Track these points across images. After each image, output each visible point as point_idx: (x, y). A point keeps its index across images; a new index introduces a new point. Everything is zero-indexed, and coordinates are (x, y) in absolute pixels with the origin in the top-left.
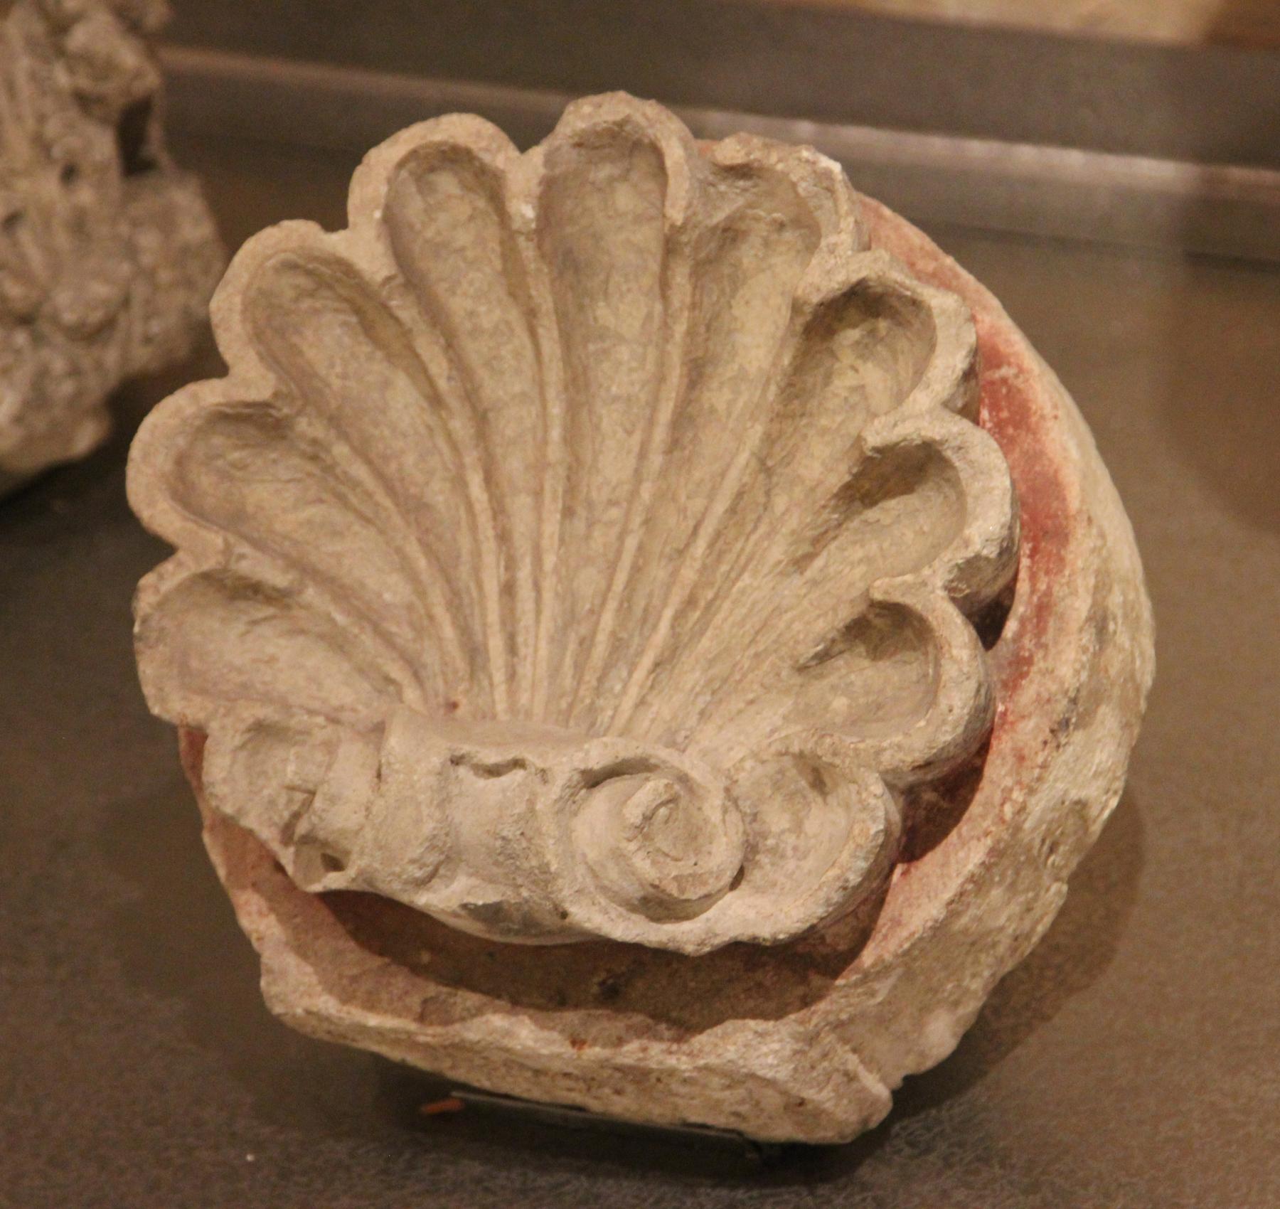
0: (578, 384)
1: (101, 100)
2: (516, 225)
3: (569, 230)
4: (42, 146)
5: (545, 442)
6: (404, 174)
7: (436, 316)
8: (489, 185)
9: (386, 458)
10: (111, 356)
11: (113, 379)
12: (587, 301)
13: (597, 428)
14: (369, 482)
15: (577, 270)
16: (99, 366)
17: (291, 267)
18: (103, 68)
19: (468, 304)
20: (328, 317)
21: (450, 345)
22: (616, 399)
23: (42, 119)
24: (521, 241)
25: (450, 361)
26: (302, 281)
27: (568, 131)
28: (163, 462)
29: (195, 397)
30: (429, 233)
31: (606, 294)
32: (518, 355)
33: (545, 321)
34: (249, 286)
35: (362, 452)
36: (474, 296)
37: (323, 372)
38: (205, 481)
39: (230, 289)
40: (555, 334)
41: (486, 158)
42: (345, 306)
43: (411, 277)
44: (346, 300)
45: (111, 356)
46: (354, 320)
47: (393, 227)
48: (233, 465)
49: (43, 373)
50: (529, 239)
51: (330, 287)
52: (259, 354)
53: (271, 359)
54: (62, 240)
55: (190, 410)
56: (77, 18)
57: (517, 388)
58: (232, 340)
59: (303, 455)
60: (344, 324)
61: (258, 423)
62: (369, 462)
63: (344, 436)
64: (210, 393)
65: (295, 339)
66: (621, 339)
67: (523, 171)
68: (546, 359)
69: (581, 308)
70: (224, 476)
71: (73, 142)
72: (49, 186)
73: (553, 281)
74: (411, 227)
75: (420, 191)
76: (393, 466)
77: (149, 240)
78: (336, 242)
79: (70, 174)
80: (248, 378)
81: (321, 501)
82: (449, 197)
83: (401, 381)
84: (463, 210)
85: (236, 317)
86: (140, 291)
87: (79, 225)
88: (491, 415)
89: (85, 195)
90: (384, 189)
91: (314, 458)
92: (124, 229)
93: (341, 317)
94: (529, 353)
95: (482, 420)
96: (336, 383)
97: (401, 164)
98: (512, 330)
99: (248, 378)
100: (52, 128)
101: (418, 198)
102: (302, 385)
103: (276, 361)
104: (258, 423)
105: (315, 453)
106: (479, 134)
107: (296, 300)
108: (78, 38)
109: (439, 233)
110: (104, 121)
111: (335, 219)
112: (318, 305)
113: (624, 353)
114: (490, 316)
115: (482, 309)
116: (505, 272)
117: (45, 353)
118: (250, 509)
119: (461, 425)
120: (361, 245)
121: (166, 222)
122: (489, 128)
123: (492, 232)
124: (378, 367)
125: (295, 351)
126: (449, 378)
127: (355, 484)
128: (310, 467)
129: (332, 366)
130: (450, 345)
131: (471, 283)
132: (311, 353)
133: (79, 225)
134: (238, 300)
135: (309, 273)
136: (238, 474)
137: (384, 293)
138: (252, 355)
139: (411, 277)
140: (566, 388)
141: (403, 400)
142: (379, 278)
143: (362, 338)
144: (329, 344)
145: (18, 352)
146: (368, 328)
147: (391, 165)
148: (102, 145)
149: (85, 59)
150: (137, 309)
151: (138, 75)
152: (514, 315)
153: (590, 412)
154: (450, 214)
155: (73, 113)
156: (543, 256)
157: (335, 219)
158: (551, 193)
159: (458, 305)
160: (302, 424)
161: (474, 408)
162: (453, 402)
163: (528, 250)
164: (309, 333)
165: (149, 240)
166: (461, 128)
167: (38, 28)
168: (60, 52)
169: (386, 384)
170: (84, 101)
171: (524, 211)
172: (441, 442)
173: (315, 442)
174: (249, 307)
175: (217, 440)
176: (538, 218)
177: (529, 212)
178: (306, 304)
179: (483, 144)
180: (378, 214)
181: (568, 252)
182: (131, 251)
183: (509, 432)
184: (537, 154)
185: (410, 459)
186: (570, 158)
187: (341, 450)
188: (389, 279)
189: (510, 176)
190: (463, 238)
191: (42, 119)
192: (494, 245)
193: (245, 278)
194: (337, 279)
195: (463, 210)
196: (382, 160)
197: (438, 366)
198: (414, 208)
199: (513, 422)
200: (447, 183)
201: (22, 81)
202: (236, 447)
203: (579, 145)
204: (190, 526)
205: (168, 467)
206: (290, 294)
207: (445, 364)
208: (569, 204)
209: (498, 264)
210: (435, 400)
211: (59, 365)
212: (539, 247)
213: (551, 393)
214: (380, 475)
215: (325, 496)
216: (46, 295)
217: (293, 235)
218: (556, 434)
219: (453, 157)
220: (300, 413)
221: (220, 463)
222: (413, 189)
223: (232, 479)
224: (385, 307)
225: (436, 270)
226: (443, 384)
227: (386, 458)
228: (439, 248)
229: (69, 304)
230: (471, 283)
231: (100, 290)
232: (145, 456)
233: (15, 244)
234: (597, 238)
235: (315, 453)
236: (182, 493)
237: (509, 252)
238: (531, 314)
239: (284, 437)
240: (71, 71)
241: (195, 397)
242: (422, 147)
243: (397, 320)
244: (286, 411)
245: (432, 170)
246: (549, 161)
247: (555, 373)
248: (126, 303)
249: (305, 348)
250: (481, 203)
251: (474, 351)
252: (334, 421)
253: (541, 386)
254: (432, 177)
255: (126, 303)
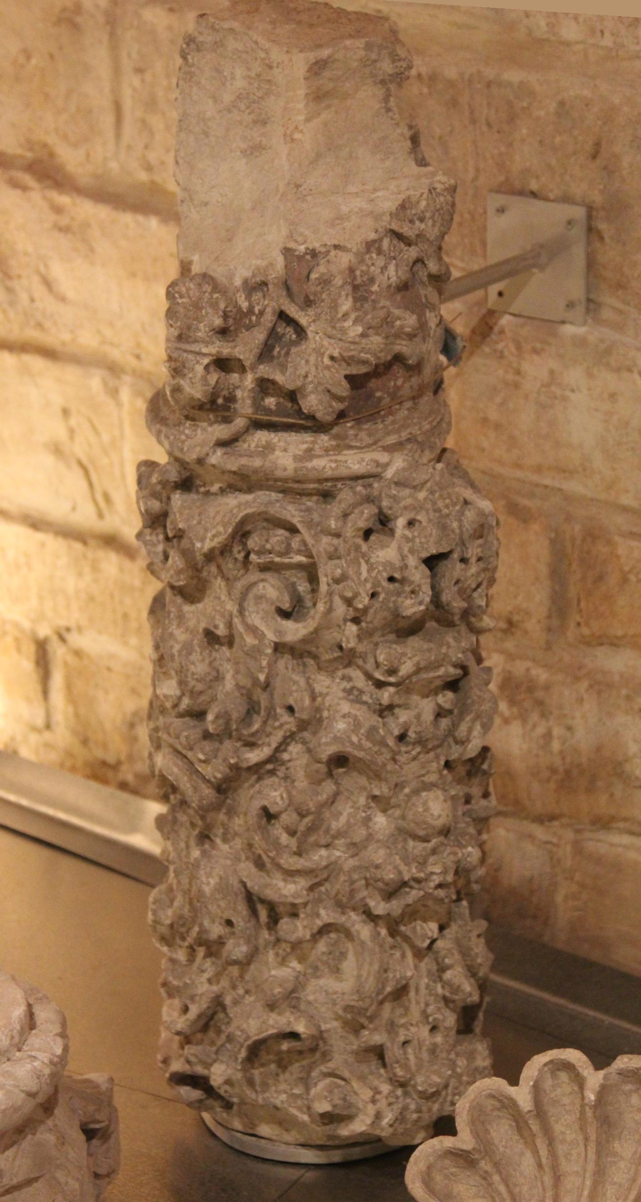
0: (600, 1174)
1: (454, 1001)
2: (586, 1101)
3: (609, 1108)
4: (425, 1015)
5: (581, 1195)
6: (546, 1069)
7: (547, 1130)
8: (580, 1082)
9: (515, 1185)
10: (436, 1107)
11: (434, 1118)
12: (611, 1139)
13: (604, 1194)
14: (505, 1194)
15: (609, 1126)
16: (430, 1110)
17: (492, 1096)
18: (457, 990)
19: (563, 1129)
20: (503, 1121)
21: (551, 1143)
22: (615, 1183)
23: (427, 1005)
24: (587, 1109)
25: (549, 1151)
26: (497, 1104)
27: (616, 1067)
28: (422, 1166)
29: (441, 1141)
30: (552, 1095)
31: (620, 1138)
32: (579, 1155)
33: (592, 1145)
34: (474, 1100)
35: (505, 1181)
36: (565, 1125)
37: (496, 1142)
38: (438, 1178)
39: (466, 1100)
40: (594, 1150)
41: (580, 1070)
42: (510, 1117)
43: (539, 1111)
44: (513, 1116)
45: (436, 1107)
46: (514, 1124)
47: (537, 1090)
48: (452, 1174)
49: (405, 1108)
50: (590, 1108)
51: (506, 1108)
52: (471, 1130)
53: (476, 1134)
54: (425, 1055)
55: (438, 1147)
56: (448, 967)
57: (575, 1169)
58: (461, 1123)
59: (481, 1176)
60: (510, 1125)
61: (465, 1159)
62: (507, 1186)
63: (500, 1173)
64: (447, 1142)
65: (489, 1127)
66: (622, 1158)
67: (594, 1079)
68: (588, 1160)
69: (608, 1141)
70: (446, 1177)
71: (438, 1016)
72: (425, 1031)
73: (597, 1128)
74: (545, 1091)
75: (552, 1077)
76: (517, 1190)
77: (461, 1062)
78: (512, 1091)
79: (434, 1029)
80: (464, 1139)
81: (485, 1197)
82: (563, 1082)
83: (528, 1154)
84: (568, 1089)
85: (465, 1112)
86: (453, 1082)
87: (433, 1050)
88: (562, 1178)
89: (439, 1039)
90: (536, 1073)
91: (485, 1179)
92: (453, 1056)
93: (510, 1122)
94: (583, 1155)
95: (557, 1179)
96: (501, 1149)
97: (545, 1065)
98: (578, 1144)
99: (464, 1139)
100: (430, 1010)
101: (550, 1080)
102: (486, 1147)
103: (478, 1136)
104: (465, 1159)
105: (485, 1176)
106: (579, 1059)
107: (492, 1110)
108: (448, 975)
109: (556, 1096)
110: (453, 1010)
111: (514, 1081)
112: (501, 1114)
113: (622, 1164)
114: (570, 1136)
115: (568, 1132)
116: (580, 1119)
117: (408, 1100)
118: (454, 1194)
119: (548, 1179)
120: (521, 1096)
121: (471, 1056)
122: (584, 1058)
123: (578, 1101)
124: (521, 1146)
125: (487, 1131)
126: (547, 1158)
127: (500, 1194)
128: (483, 1182)
129: (501, 1141)
130: (551, 1143)
131: (565, 1120)
132: (493, 1134)
133: (433, 1050)
134: (468, 1105)
135: (500, 1101)
136: (453, 1178)
137: (527, 1116)
138: (468, 1130)
139: (539, 1111)
140: (594, 1174)
141: (527, 1162)
142: (526, 1110)
143: (516, 1133)
144: (502, 1132)
145: (397, 1098)
146: (519, 1129)
147: (541, 1064)
148: (450, 1020)
149: (446, 984)
150: (450, 1089)
151: (470, 995)
152: (581, 1138)
153: (603, 1186)
154: (561, 1089)
155: (442, 1004)
156: (595, 1117)
157: (514, 1081)
158: (603, 1091)
159: (558, 1128)
160: (482, 1164)
161: (555, 1173)
162: (547, 1169)
163: (589, 1113)
164: (495, 1126)
165: (461, 1062)
166: (573, 1055)
167: (435, 968)
168: (440, 979)
169: (522, 1154)
170: (446, 1000)
171: (591, 1097)
172: (539, 1184)
173: (486, 1172)
174: (472, 1109)
175: (447, 1162)
176: (596, 1101)
177: (593, 1097)
178: (496, 1113)
179: (580, 1064)
180: (531, 1083)
181: (607, 1117)
182: (453, 1065)
183: (568, 1187)
184: (601, 1073)
185: (525, 1188)
186: (614, 1078)
187: (496, 1178)
188: (530, 1111)
189: (588, 1080)
190: (566, 1100)
191: (427, 1005)
192: (578, 1106)
193: (472, 1097)
194: (508, 1105)
195: (568, 1089)
196: (540, 1060)
197: (544, 1152)
198: (548, 1083)
199: (570, 1183)
200: (563, 1076)
201: (422, 986)
202: (455, 1167)
203: (620, 1074)
204: (427, 1196)
205: (424, 1169)
206: (490, 1107)
207: (546, 1152)
208: (611, 1097)
209: (578, 1115)
210: (540, 1166)
211: (413, 1107)
212: (594, 1112)
213: (588, 1175)
214: (510, 1192)
215: (487, 1196)
216: (413, 1076)
217: (499, 1083)
218: (586, 1193)
219: (568, 1066)
220: (482, 1159)
221: (446, 1171)
222: (549, 1076)
223: (450, 1180)
224: (526, 1122)
225: (552, 1111)
226: (544, 1161)
227: (515, 1185)
228: (555, 1102)
229: (421, 1082)
230: (565, 1120)
231: (436, 1079)
232: (415, 1163)
233: (405, 1053)
234: (620, 1114)
235: (485, 1176)
236: (427, 1181)
237: (582, 1112)
238: (586, 1139)
239: (475, 1167)
240: (443, 987)
241: (441, 1141)
242: (557, 1060)
243: (530, 1129)
244: (477, 1156)
245: (558, 1070)
246: (605, 1078)
247: (591, 1167)
248: (446, 1086)
249: (491, 1131)
250: (576, 1088)
251: (561, 1149)
252: (496, 1165)
253: (585, 1171)
254: (558, 1073)
255: (446, 1086)
